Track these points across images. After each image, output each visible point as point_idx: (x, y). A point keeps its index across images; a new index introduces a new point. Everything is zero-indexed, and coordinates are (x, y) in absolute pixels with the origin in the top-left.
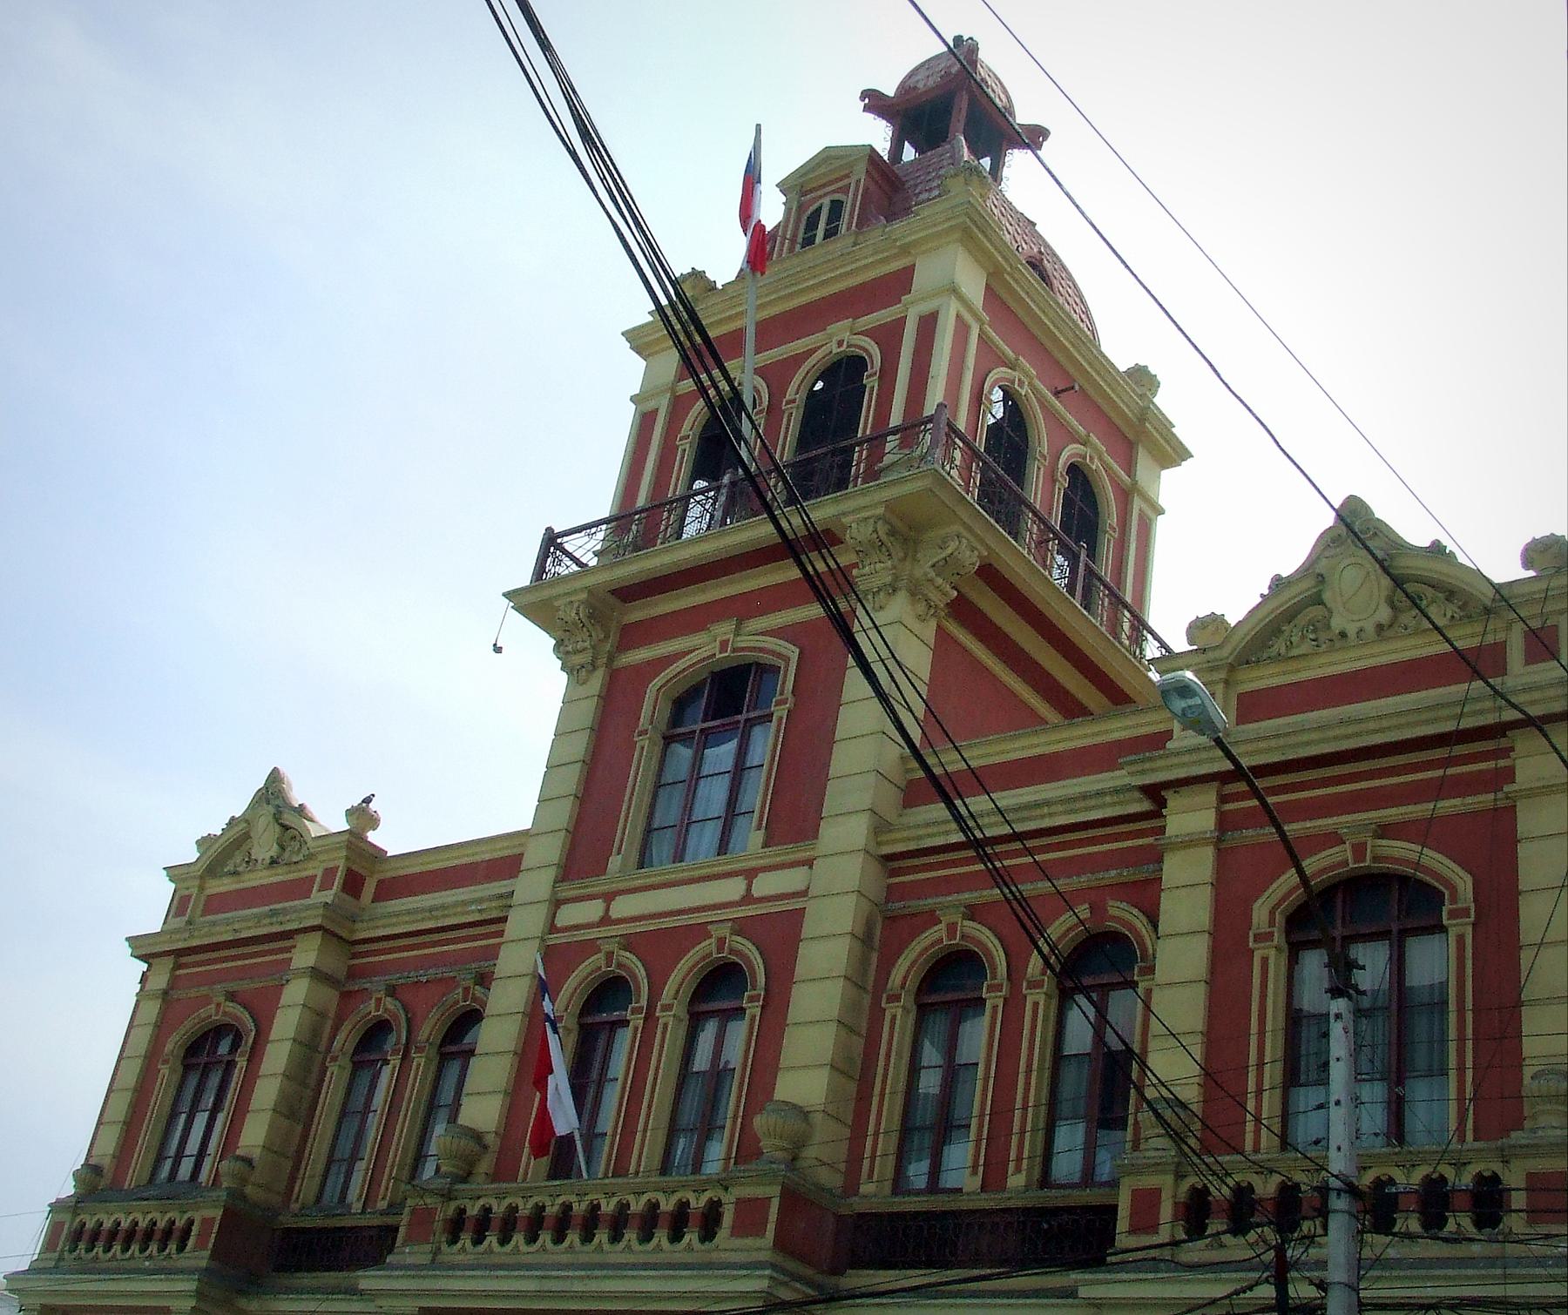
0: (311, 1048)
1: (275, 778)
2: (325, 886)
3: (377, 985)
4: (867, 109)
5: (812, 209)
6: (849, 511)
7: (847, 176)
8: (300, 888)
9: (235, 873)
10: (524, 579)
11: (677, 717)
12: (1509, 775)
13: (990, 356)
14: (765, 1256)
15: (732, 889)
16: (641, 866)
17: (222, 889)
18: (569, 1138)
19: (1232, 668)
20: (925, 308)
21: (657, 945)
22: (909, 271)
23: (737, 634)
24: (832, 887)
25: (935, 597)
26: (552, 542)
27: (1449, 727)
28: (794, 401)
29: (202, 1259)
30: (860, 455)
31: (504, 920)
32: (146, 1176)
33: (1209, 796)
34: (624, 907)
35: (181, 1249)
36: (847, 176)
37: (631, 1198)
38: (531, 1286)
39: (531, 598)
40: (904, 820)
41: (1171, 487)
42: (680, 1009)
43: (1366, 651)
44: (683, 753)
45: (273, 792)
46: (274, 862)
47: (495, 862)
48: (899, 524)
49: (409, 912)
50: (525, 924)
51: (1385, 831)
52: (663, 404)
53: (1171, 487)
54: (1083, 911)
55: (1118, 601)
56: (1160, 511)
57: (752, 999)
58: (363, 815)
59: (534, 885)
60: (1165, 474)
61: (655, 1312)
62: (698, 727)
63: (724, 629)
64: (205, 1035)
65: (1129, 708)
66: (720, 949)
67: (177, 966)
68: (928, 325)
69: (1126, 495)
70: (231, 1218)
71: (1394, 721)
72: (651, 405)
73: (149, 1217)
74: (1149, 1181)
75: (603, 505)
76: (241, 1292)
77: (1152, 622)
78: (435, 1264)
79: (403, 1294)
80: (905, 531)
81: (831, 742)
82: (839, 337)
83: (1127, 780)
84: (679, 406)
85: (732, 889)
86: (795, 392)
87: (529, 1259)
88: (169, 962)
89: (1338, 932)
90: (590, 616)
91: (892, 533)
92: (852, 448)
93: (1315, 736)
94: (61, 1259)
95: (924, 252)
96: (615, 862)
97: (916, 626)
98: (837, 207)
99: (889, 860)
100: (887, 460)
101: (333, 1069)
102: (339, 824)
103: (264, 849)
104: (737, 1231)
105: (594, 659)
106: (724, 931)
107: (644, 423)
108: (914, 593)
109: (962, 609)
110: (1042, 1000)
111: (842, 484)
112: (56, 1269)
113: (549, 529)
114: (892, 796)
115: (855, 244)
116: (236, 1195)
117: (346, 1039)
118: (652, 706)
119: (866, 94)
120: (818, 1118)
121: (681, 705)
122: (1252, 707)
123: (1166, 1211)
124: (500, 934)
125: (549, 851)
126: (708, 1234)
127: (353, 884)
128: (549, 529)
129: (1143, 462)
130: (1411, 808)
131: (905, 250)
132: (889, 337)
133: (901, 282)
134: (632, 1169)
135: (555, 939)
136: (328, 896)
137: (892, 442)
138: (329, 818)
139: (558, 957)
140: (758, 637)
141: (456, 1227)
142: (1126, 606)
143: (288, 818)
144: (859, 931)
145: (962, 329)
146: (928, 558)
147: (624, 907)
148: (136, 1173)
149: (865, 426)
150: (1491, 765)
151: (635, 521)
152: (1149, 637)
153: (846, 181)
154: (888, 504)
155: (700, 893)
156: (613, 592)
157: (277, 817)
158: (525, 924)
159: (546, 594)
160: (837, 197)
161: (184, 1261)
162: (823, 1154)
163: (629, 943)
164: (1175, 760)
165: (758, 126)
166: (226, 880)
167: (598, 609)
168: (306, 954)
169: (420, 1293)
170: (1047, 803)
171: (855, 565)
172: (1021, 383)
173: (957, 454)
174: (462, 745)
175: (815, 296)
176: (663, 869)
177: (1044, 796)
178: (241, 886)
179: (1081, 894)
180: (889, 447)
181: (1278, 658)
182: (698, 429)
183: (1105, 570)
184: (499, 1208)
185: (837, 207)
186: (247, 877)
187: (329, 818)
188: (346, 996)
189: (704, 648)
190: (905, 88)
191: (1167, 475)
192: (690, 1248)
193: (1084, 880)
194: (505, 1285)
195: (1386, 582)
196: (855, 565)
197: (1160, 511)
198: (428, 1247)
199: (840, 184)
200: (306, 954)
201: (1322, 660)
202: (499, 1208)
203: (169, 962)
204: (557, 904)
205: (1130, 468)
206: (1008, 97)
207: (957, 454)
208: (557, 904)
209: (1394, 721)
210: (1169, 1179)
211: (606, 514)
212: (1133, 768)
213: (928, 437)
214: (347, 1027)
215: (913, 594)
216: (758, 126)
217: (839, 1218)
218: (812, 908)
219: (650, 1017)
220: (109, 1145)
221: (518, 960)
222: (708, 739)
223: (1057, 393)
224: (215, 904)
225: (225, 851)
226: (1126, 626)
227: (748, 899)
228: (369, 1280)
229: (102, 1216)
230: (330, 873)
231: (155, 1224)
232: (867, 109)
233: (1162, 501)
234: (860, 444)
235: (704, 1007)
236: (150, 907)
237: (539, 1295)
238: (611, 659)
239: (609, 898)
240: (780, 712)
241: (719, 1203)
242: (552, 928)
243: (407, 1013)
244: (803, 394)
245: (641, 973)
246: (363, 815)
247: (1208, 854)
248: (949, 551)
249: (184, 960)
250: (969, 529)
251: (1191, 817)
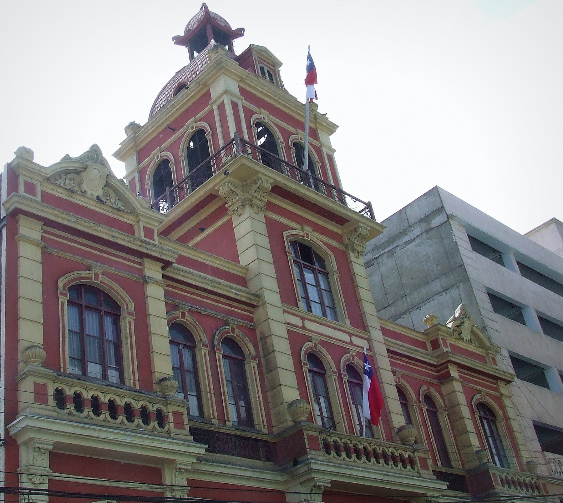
6: (216, 183)
13: (249, 113)
16: (389, 351)
18: (188, 480)
20: (218, 102)
28: (182, 155)
30: (213, 162)
41: (335, 141)
44: (87, 159)
52: (136, 175)
53: (335, 140)
55: (329, 186)
56: (334, 151)
61: (2, 236)
65: (348, 224)
68: (221, 107)
77: (345, 189)
82: (190, 126)
86: (182, 151)
95: (211, 83)
97: (256, 216)
100: (224, 160)
106: (317, 342)
109: (270, 206)
110: (256, 366)
111: (210, 175)
119: (174, 38)
123: (171, 419)
129: (322, 135)
132: (209, 118)
137: (223, 153)
142: (333, 187)
145: (235, 106)
149: (212, 151)
152: (346, 196)
165: (309, 46)
173: (248, 149)
180: (222, 155)
182: (151, 179)
183: (320, 176)
190: (187, 30)
191: (332, 137)
197: (334, 151)
207: (248, 149)
213: (235, 146)
215: (251, 206)
216: (309, 46)
226: (335, 194)
233: (333, 147)
234: (211, 159)
244: (185, 151)
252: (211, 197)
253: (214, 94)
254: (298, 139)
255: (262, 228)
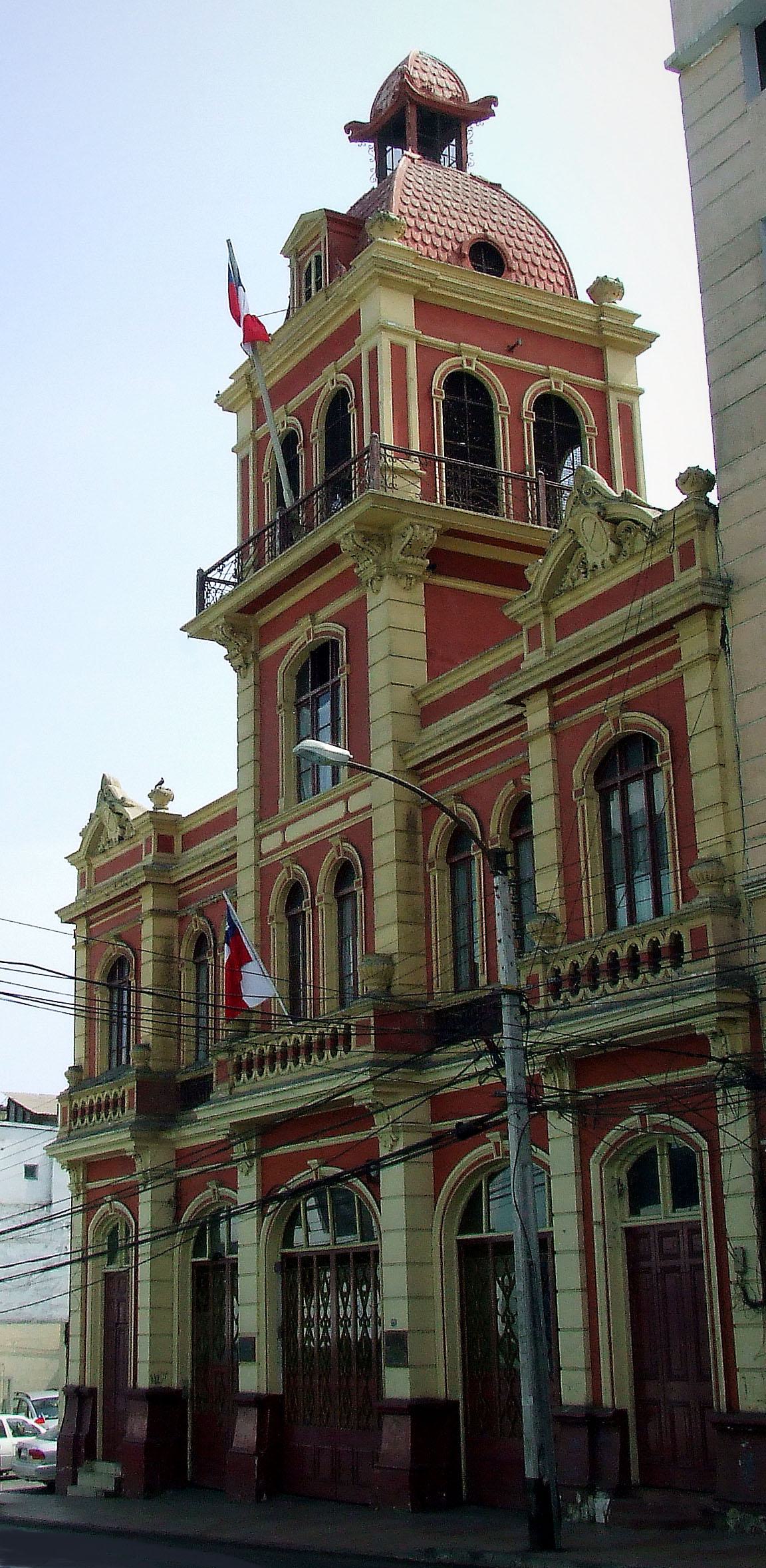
0: (166, 959)
1: (105, 781)
2: (148, 852)
3: (191, 911)
4: (351, 139)
5: (307, 265)
7: (317, 237)
8: (134, 856)
9: (104, 851)
10: (191, 613)
11: (301, 691)
12: (677, 655)
14: (370, 1057)
15: (337, 811)
17: (102, 863)
19: (544, 603)
21: (309, 856)
22: (355, 320)
23: (314, 625)
24: (382, 803)
25: (412, 570)
26: (203, 579)
27: (629, 636)
29: (130, 1114)
31: (235, 856)
32: (106, 1067)
33: (543, 699)
34: (293, 833)
35: (123, 1112)
36: (317, 237)
37: (637, 941)
38: (269, 1100)
39: (198, 626)
40: (425, 737)
42: (331, 899)
43: (609, 576)
45: (106, 795)
46: (121, 838)
47: (219, 819)
48: (368, 529)
49: (454, 728)
50: (246, 856)
51: (627, 706)
52: (250, 449)
54: (510, 785)
56: (639, 393)
57: (662, 759)
58: (160, 795)
59: (245, 829)
60: (641, 359)
62: (311, 693)
63: (306, 622)
64: (114, 968)
66: (617, 728)
67: (89, 923)
68: (373, 355)
69: (600, 398)
70: (381, 1016)
71: (612, 633)
72: (243, 454)
73: (648, 937)
74: (696, 923)
75: (232, 541)
76: (167, 1129)
78: (232, 1095)
79: (218, 1118)
80: (376, 535)
81: (367, 696)
82: (329, 379)
83: (498, 699)
84: (260, 445)
85: (337, 811)
87: (262, 1084)
88: (83, 922)
89: (619, 778)
90: (232, 632)
91: (367, 537)
92: (348, 469)
93: (577, 651)
94: (71, 1130)
96: (281, 802)
97: (405, 596)
98: (318, 258)
99: (417, 771)
101: (434, 873)
102: (149, 806)
103: (113, 833)
104: (358, 1044)
105: (245, 659)
107: (243, 464)
108: (396, 574)
112: (69, 1138)
113: (200, 571)
114: (411, 723)
115: (327, 298)
116: (144, 1071)
117: (185, 950)
118: (283, 686)
119: (348, 128)
120: (396, 958)
121: (301, 678)
122: (566, 625)
124: (235, 866)
125: (246, 805)
126: (677, 963)
127: (165, 844)
128: (200, 571)
129: (613, 361)
130: (637, 688)
131: (351, 300)
132: (353, 370)
133: (352, 328)
134: (587, 934)
135: (263, 863)
136: (148, 860)
138: (140, 804)
139: (265, 876)
140: (324, 624)
141: (238, 1068)
143: (119, 808)
144: (402, 825)
145: (399, 353)
146: (399, 545)
147: (293, 833)
148: (100, 1066)
149: (354, 451)
150: (652, 657)
151: (252, 550)
153: (317, 243)
154: (357, 522)
155: (321, 819)
156: (240, 611)
157: (112, 809)
158: (246, 856)
159: (207, 620)
160: (317, 253)
161: (353, 1058)
162: (405, 982)
163: (297, 858)
164: (528, 676)
166: (102, 856)
167: (239, 618)
168: (147, 902)
169: (226, 1116)
170: (477, 717)
171: (356, 565)
172: (469, 363)
174: (188, 737)
175: (316, 343)
176: (311, 801)
177: (472, 713)
178: (112, 858)
179: (501, 779)
181: (571, 589)
184: (583, 962)
185: (318, 258)
186: (111, 852)
187: (140, 804)
188: (182, 920)
189: (298, 638)
190: (375, 112)
192: (341, 1059)
193: (507, 765)
194: (647, 1015)
195: (606, 525)
196: (356, 565)
197: (639, 393)
198: (227, 1085)
199: (313, 247)
200: (147, 902)
201: (589, 587)
202: (302, 1039)
203: (83, 922)
204: (259, 838)
205: (602, 375)
206: (459, 82)
208: (259, 838)
209: (608, 635)
210: (540, 967)
211: (235, 546)
212: (499, 691)
214: (184, 943)
217: (428, 1015)
218: (374, 815)
219: (314, 908)
220: (82, 1052)
221: (246, 882)
222: (316, 703)
223: (510, 351)
224: (101, 874)
225: (94, 838)
227: (348, 815)
228: (202, 1112)
229: (84, 1099)
230: (148, 840)
231: (577, 966)
232: (351, 139)
235: (341, 893)
236: (65, 887)
237: (277, 1104)
238: (255, 656)
239: (283, 828)
240: (343, 677)
241: (679, 936)
242: (261, 856)
243: (211, 925)
245: (652, 722)
246: (160, 795)
247: (548, 738)
248: (408, 538)
249: (93, 917)
250: (417, 517)
251: (538, 716)
252: (331, 552)
253: (366, 322)
254: (550, 387)
255: (417, 619)
